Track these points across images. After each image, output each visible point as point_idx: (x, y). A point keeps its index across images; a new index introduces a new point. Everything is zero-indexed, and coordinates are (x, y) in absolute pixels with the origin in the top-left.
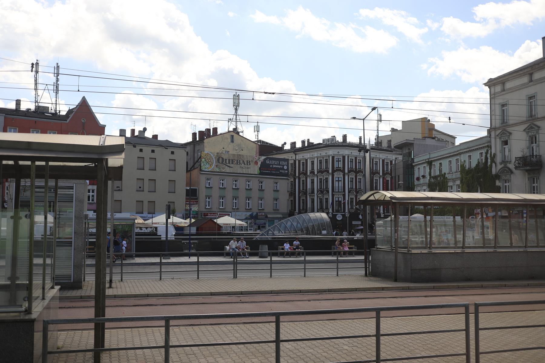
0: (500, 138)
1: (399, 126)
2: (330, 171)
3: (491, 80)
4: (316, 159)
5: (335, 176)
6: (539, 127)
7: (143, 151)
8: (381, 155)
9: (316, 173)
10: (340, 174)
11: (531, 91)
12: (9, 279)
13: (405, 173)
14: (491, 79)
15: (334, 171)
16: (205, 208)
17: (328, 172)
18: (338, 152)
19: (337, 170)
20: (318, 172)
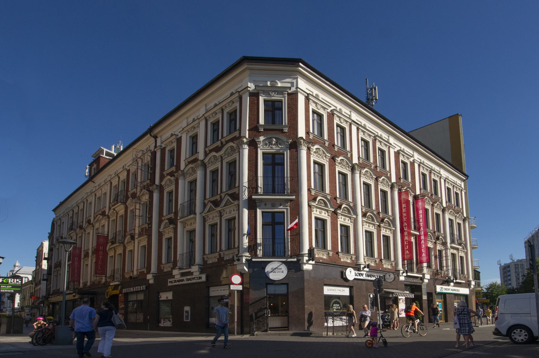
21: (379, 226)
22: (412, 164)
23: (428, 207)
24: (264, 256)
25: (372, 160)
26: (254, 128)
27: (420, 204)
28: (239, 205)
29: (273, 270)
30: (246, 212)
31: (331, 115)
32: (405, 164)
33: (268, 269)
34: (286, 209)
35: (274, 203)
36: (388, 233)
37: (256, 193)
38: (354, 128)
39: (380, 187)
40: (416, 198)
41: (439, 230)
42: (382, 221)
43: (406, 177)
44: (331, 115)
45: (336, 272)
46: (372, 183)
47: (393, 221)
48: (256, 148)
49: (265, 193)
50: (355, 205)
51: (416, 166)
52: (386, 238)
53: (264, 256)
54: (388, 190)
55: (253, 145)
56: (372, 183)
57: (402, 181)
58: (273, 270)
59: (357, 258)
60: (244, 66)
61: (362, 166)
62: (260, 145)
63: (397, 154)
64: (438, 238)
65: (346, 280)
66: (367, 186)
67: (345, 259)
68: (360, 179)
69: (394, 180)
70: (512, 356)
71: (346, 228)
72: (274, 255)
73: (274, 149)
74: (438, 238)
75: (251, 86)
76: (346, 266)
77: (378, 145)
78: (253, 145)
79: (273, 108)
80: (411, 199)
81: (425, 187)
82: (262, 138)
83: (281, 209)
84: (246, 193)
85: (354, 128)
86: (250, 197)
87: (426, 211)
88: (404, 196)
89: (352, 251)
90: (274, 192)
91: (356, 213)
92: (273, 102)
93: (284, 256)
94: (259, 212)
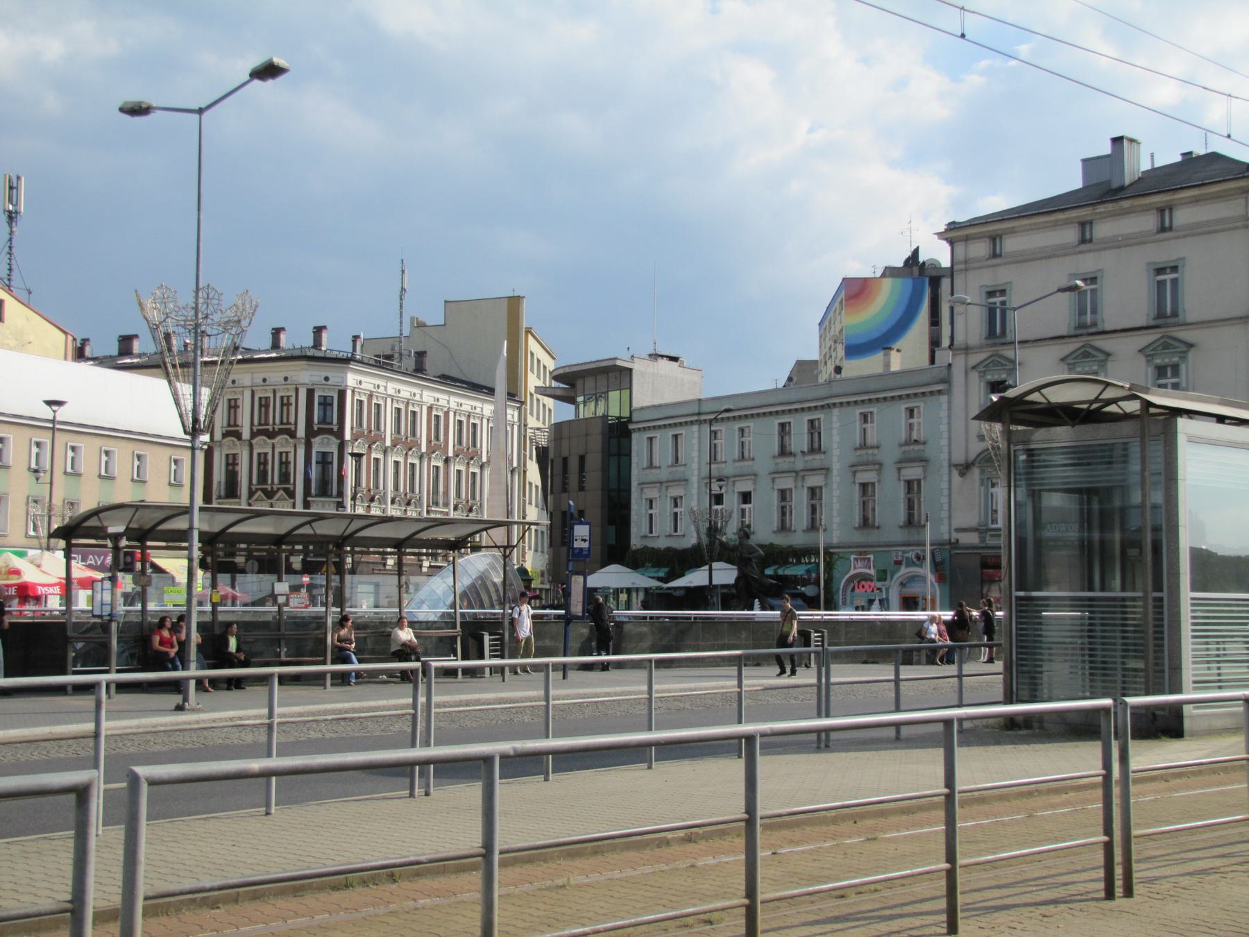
0: (983, 374)
1: (435, 316)
2: (301, 432)
3: (953, 226)
4: (248, 394)
5: (316, 449)
6: (1108, 354)
7: (420, 349)
8: (425, 393)
9: (246, 434)
10: (328, 444)
11: (1087, 262)
12: (948, 861)
13: (607, 453)
14: (954, 223)
15: (311, 433)
16: (27, 536)
17: (293, 434)
18: (327, 379)
19: (321, 431)
20: (253, 435)
25: (365, 426)
38: (389, 400)
39: (374, 455)
44: (371, 396)
46: (401, 460)
51: (451, 414)
63: (430, 408)
66: (397, 463)
85: (389, 400)
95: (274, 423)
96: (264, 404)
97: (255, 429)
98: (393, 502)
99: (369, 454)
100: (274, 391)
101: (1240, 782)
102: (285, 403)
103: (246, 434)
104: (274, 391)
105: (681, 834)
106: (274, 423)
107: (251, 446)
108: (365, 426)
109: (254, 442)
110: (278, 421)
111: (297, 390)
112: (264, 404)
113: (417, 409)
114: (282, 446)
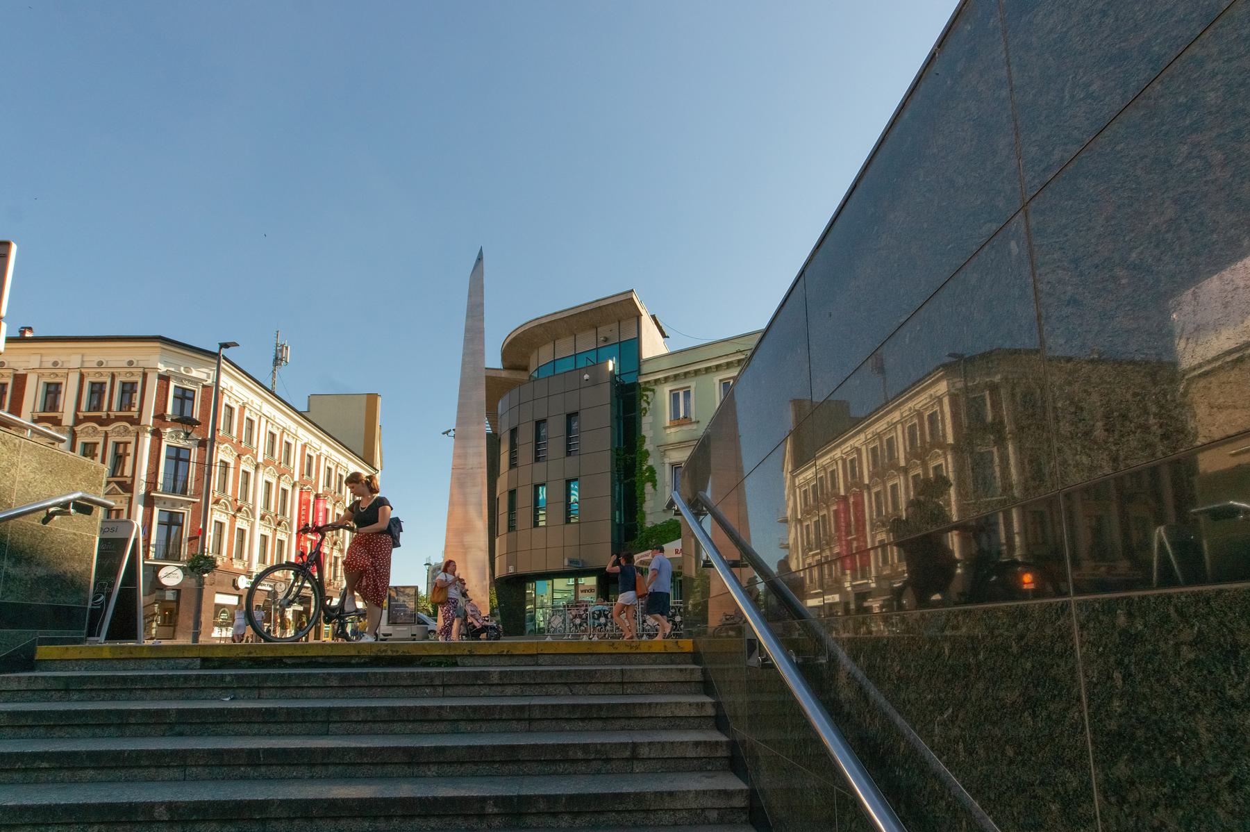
4: (74, 379)
9: (68, 420)
20: (77, 421)
21: (234, 516)
22: (319, 457)
23: (329, 507)
24: (156, 559)
25: (235, 433)
26: (160, 416)
27: (321, 505)
28: (131, 499)
29: (167, 575)
30: (141, 509)
31: (243, 407)
32: (310, 457)
33: (162, 573)
34: (187, 512)
35: (174, 503)
36: (284, 538)
37: (155, 489)
38: (263, 420)
39: (243, 467)
40: (317, 497)
41: (284, 513)
42: (239, 510)
43: (309, 474)
44: (243, 407)
45: (228, 580)
46: (274, 481)
47: (290, 524)
48: (160, 439)
49: (164, 492)
50: (254, 508)
51: (322, 459)
52: (281, 542)
53: (156, 559)
54: (289, 488)
55: (157, 434)
56: (274, 481)
57: (243, 445)
58: (167, 575)
59: (250, 565)
60: (158, 344)
61: (267, 464)
62: (165, 438)
63: (304, 446)
64: (335, 544)
65: (237, 588)
66: (268, 484)
67: (238, 565)
68: (263, 476)
69: (296, 478)
70: (1207, 557)
71: (242, 531)
72: (167, 557)
73: (182, 443)
74: (335, 544)
75: (162, 368)
76: (239, 574)
77: (285, 438)
78: (157, 434)
79: (184, 397)
80: (312, 498)
81: (329, 484)
82: (169, 430)
83: (181, 509)
84: (144, 487)
85: (263, 420)
86: (147, 494)
87: (327, 511)
88: (305, 496)
89: (246, 557)
90: (174, 491)
91: (254, 517)
92: (185, 390)
93: (178, 560)
94: (156, 510)
95: (110, 408)
96: (97, 390)
97: (81, 415)
98: (262, 518)
99: (275, 535)
100: (113, 376)
101: (961, 510)
102: (128, 389)
103: (68, 420)
104: (113, 376)
105: (701, 752)
106: (110, 408)
107: (74, 435)
108: (272, 509)
109: (78, 429)
110: (115, 406)
111: (145, 375)
112: (97, 390)
113: (292, 441)
114: (119, 434)
